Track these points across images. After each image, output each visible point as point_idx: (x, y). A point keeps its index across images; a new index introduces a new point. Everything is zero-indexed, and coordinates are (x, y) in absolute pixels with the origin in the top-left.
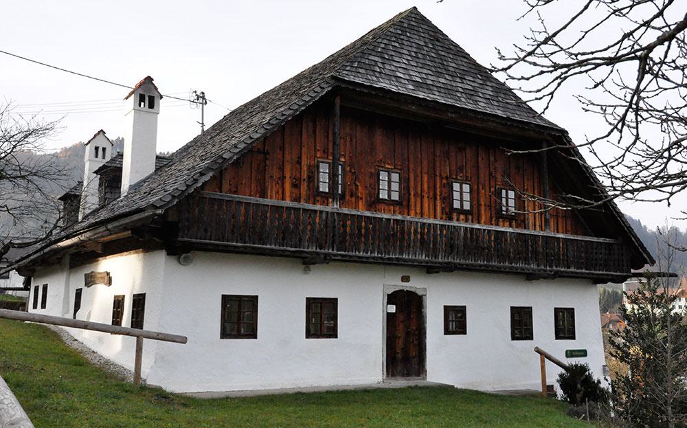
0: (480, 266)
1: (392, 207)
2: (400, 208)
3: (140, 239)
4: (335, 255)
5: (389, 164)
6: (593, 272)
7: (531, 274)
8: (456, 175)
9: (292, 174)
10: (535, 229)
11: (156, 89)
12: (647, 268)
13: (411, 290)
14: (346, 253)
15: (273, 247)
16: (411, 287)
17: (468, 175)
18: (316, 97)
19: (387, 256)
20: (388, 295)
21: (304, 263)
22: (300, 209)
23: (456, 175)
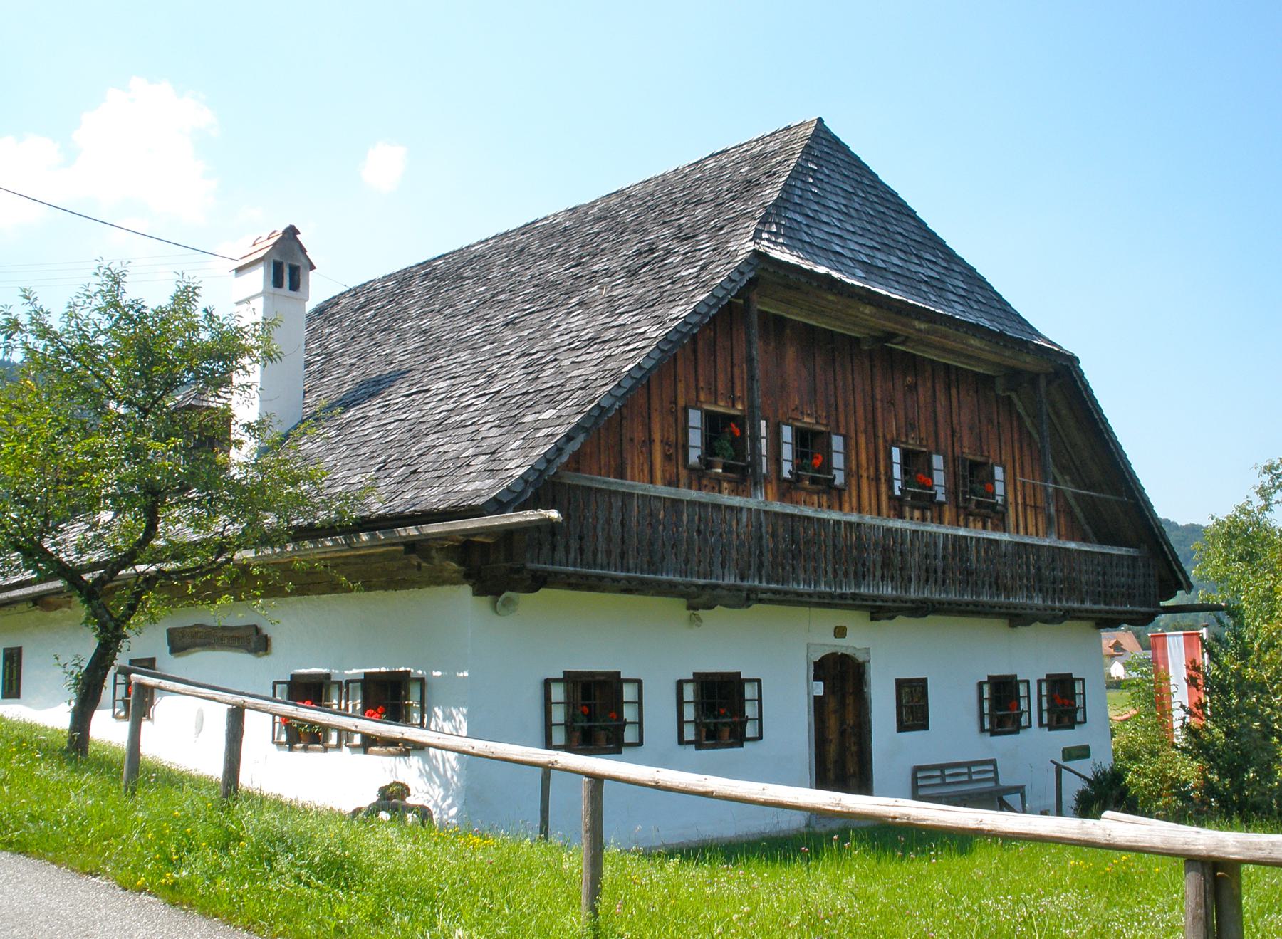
0: (967, 604)
1: (816, 497)
2: (828, 499)
3: (424, 564)
4: (765, 591)
5: (808, 415)
6: (1113, 607)
7: (1018, 615)
8: (907, 436)
9: (663, 436)
10: (1018, 532)
11: (303, 251)
12: (1180, 598)
13: (848, 652)
14: (689, 579)
15: (671, 577)
16: (847, 647)
17: (923, 435)
18: (732, 290)
19: (838, 591)
20: (815, 663)
21: (690, 607)
22: (741, 509)
23: (907, 436)
